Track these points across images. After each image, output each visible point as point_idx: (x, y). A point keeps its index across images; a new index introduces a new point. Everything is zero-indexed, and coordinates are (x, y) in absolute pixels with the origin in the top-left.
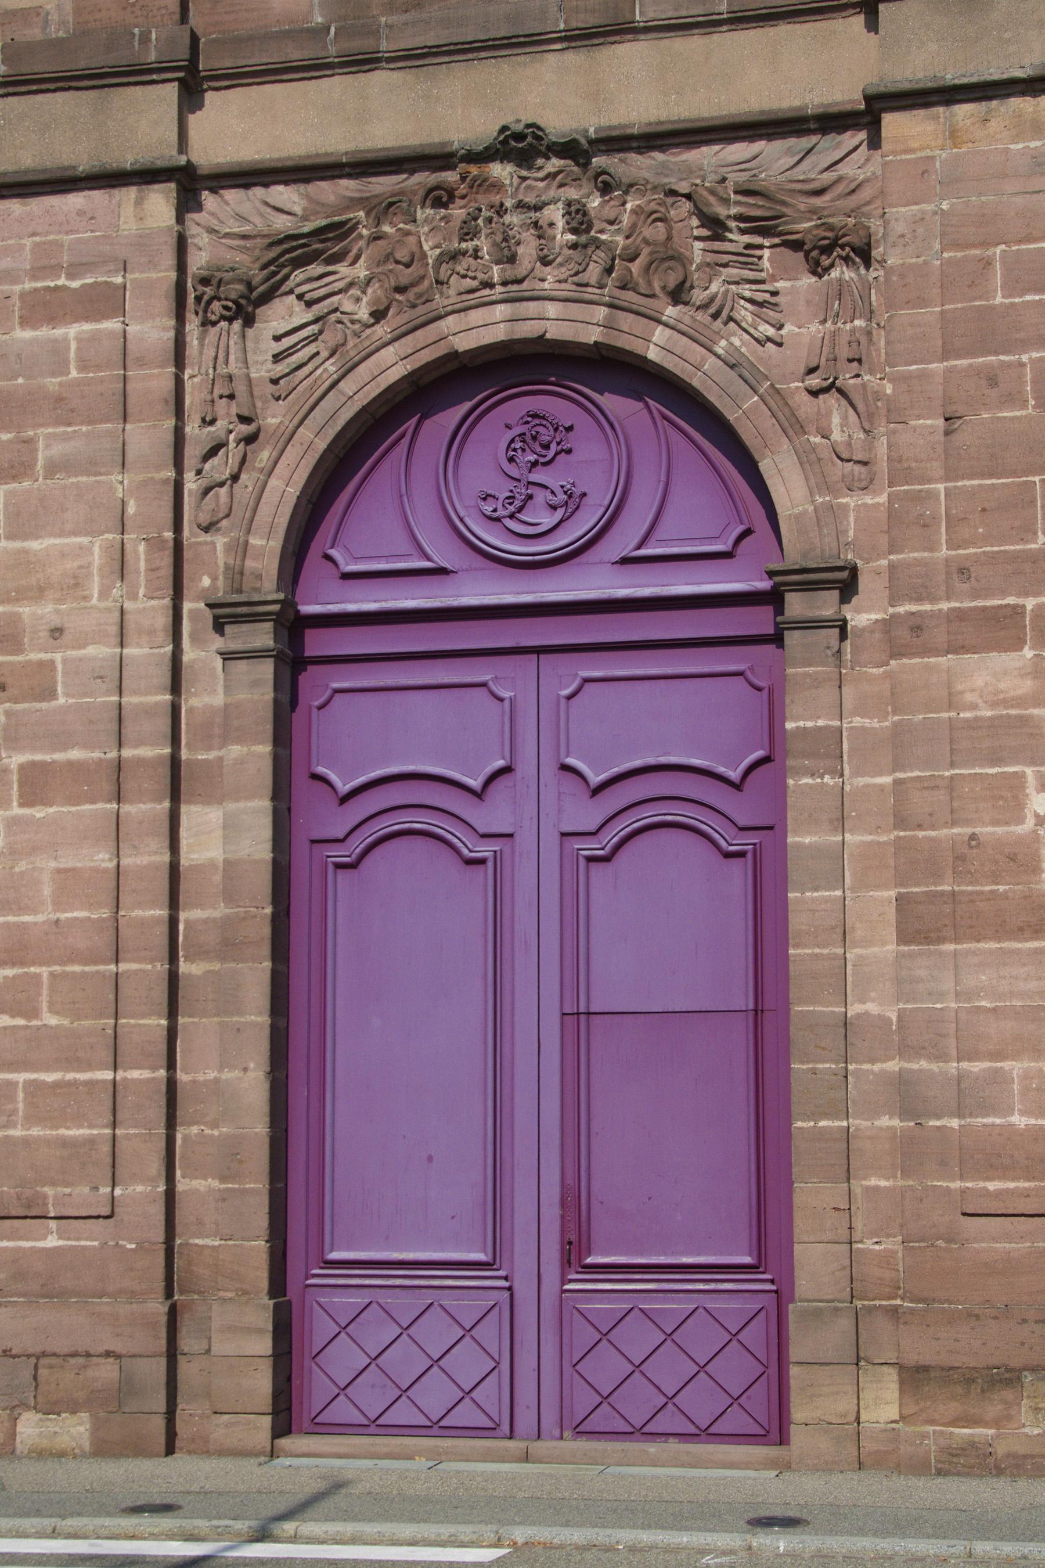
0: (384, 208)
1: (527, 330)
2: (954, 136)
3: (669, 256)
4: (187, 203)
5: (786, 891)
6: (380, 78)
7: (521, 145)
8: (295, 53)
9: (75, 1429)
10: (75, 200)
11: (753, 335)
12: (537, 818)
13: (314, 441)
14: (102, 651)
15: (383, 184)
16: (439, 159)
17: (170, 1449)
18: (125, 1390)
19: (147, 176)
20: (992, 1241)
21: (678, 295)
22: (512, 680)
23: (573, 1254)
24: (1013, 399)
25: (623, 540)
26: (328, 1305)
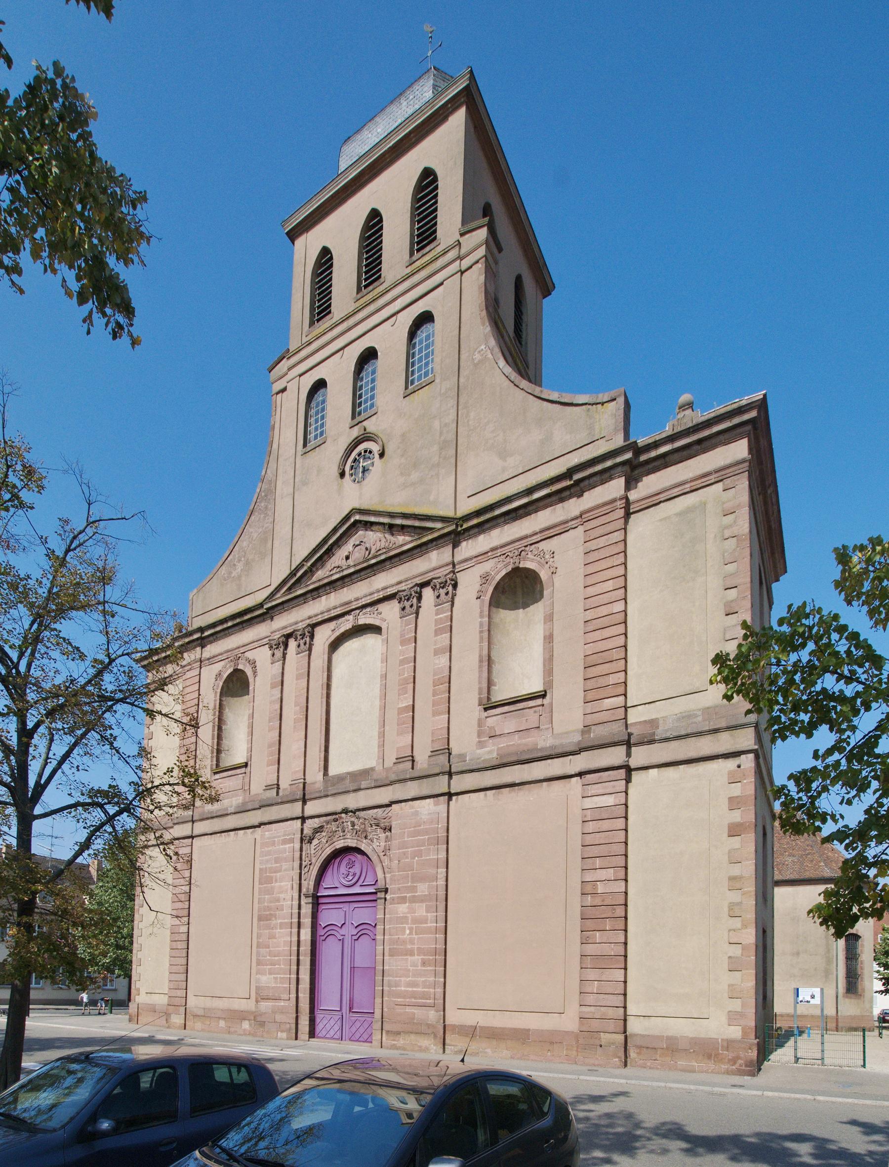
0: (328, 823)
1: (346, 845)
2: (401, 809)
3: (365, 831)
4: (303, 822)
5: (9, 1009)
6: (329, 798)
7: (346, 811)
8: (317, 795)
9: (284, 1035)
10: (289, 822)
11: (373, 846)
12: (349, 931)
13: (318, 865)
14: (290, 903)
15: (329, 818)
16: (335, 814)
17: (296, 1039)
18: (290, 1029)
19: (297, 818)
20: (399, 1010)
21: (366, 837)
22: (345, 907)
23: (350, 1009)
24: (407, 858)
25: (360, 883)
26: (319, 1016)
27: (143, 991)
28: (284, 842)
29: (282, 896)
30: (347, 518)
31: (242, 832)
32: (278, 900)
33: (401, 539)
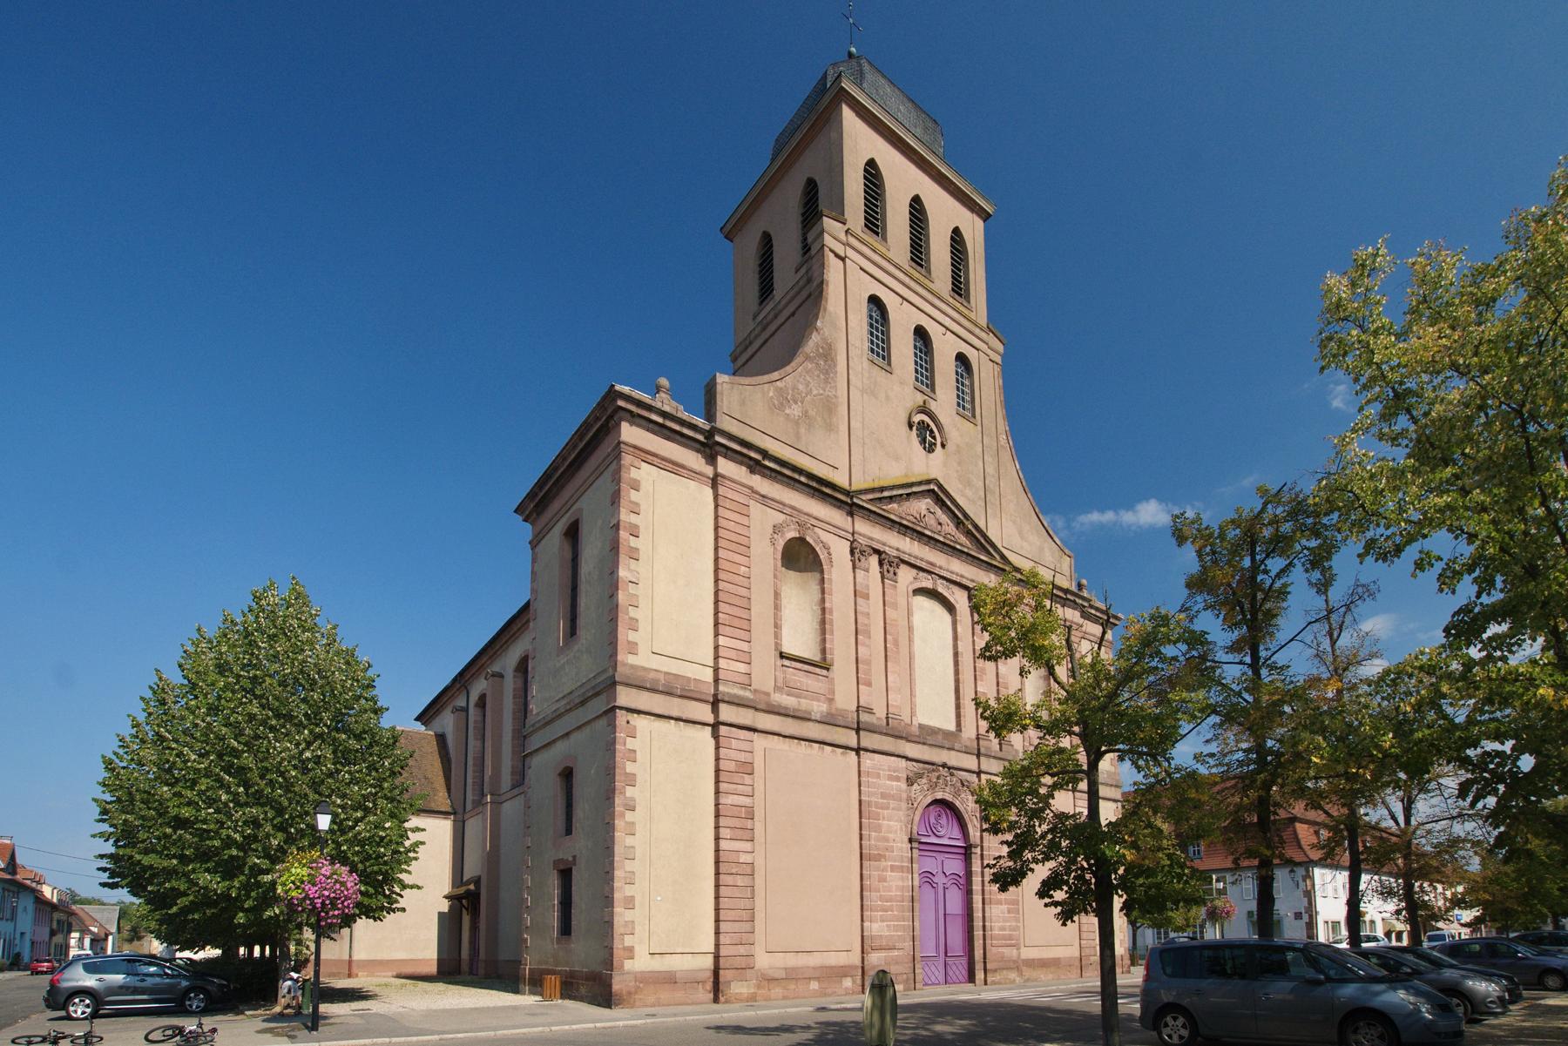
7: (944, 766)
27: (641, 952)
28: (891, 778)
29: (891, 836)
30: (929, 482)
31: (829, 749)
32: (887, 840)
33: (963, 539)
